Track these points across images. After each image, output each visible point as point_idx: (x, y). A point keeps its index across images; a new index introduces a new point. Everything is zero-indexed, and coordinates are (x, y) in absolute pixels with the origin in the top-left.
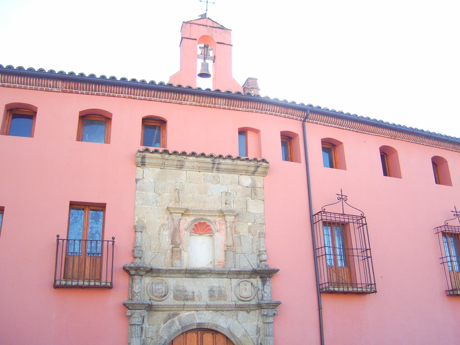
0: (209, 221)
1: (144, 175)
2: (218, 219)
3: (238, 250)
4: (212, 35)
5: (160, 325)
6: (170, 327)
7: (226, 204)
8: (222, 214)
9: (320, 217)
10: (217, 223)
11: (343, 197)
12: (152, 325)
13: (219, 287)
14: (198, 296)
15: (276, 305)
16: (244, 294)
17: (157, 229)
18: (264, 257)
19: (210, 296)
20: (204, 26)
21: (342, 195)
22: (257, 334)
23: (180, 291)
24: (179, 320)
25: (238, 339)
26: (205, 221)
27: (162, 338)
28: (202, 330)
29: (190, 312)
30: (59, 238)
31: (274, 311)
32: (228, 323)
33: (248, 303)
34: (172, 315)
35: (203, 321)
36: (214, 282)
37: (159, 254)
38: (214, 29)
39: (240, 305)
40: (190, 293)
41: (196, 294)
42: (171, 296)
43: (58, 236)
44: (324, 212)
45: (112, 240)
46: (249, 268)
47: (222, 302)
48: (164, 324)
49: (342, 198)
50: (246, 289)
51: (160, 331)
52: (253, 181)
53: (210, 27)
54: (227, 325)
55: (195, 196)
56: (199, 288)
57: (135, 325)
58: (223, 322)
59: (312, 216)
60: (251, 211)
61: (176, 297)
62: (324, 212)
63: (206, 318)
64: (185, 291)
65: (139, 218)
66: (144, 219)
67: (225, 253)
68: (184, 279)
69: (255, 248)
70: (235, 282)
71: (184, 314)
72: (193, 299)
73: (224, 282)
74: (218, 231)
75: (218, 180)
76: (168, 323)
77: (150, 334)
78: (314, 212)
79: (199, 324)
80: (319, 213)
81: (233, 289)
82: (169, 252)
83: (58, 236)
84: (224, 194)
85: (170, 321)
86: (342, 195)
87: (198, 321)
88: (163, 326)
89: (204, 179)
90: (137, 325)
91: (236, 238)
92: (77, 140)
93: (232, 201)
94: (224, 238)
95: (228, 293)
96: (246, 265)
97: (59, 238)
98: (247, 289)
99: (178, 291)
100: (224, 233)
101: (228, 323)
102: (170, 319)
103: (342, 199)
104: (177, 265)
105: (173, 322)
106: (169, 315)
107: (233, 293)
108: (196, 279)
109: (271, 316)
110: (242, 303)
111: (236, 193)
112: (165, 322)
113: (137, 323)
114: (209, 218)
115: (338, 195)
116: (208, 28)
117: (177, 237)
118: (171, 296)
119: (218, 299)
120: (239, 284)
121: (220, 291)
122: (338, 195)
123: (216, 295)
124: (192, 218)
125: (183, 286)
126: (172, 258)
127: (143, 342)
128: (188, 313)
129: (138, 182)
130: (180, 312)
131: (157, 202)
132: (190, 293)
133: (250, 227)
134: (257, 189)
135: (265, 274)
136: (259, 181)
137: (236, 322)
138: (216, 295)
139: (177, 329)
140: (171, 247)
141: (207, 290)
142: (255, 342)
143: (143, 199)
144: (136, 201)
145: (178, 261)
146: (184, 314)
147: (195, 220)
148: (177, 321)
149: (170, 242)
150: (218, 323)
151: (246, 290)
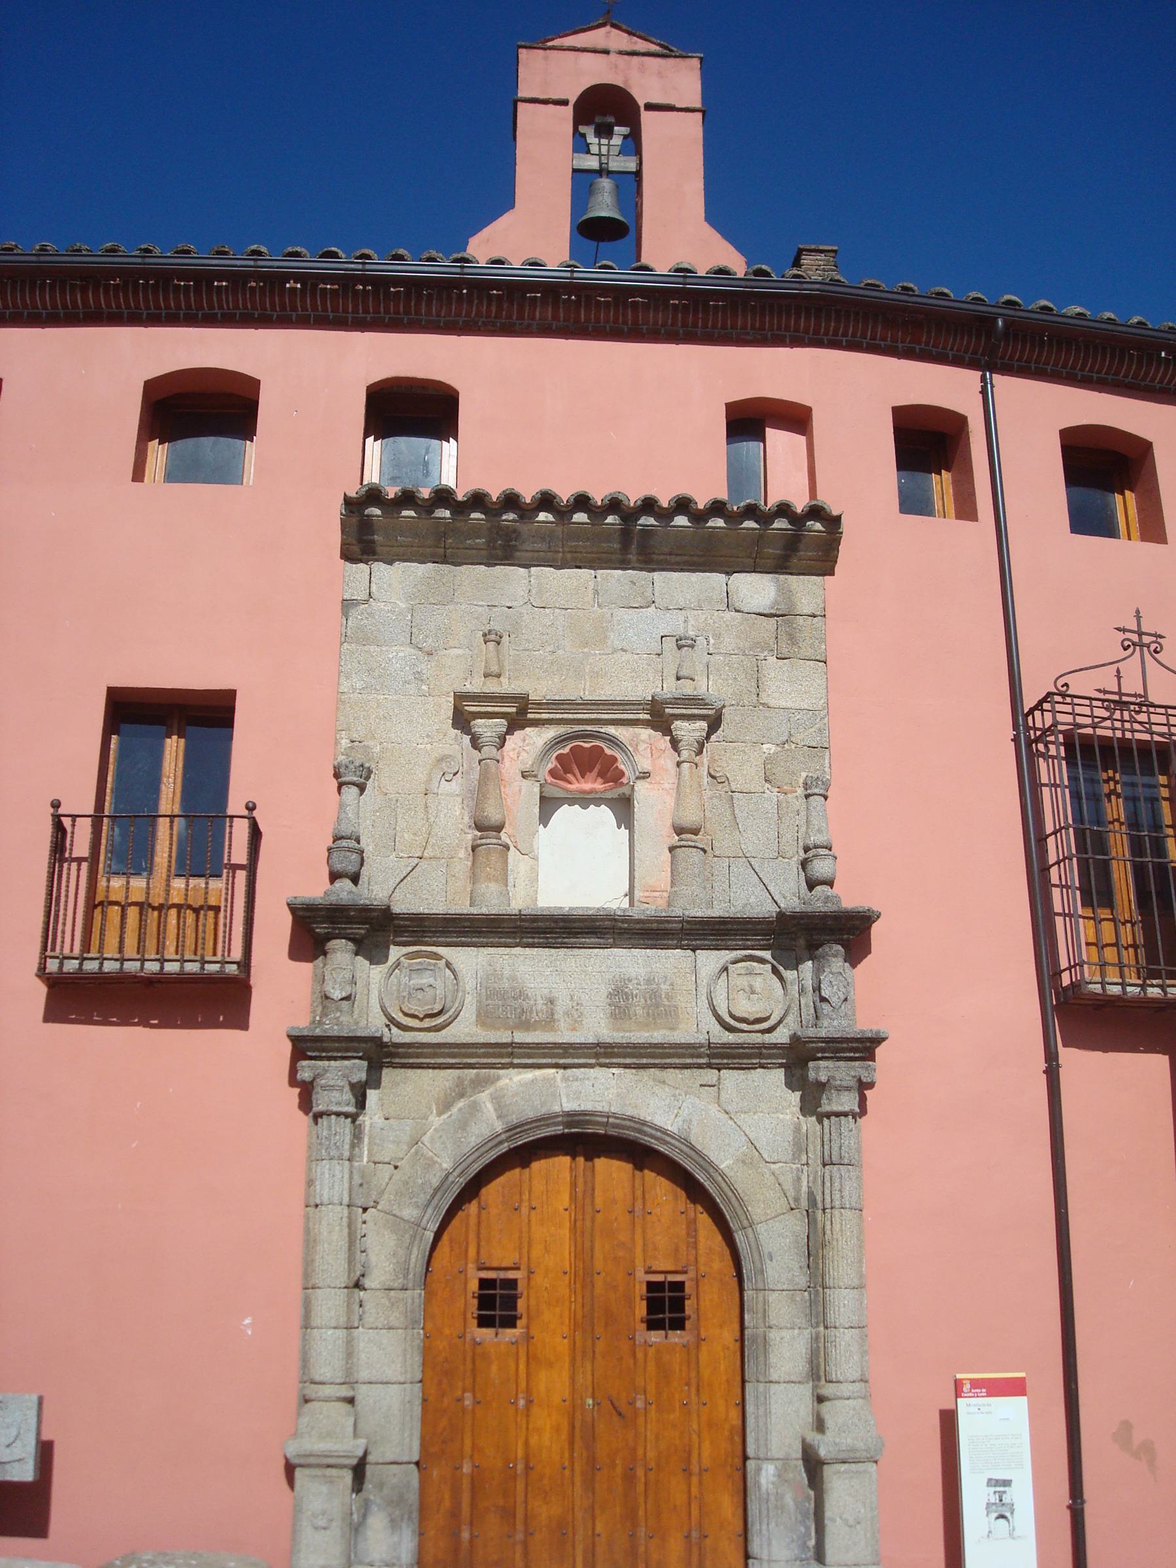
0: (613, 741)
1: (374, 588)
2: (645, 733)
3: (724, 843)
4: (626, 81)
5: (425, 1117)
6: (463, 1125)
7: (678, 679)
8: (659, 716)
9: (1048, 717)
10: (643, 747)
11: (1146, 639)
12: (398, 1118)
13: (649, 981)
14: (567, 1014)
15: (865, 1047)
16: (746, 1007)
17: (421, 775)
18: (821, 868)
19: (613, 1015)
20: (595, 51)
21: (1140, 634)
22: (795, 1157)
23: (501, 995)
24: (497, 1100)
25: (723, 1175)
26: (598, 743)
27: (430, 1164)
28: (584, 1140)
29: (538, 1073)
30: (61, 811)
31: (857, 1069)
32: (684, 1113)
33: (758, 1038)
34: (472, 1081)
35: (587, 1106)
36: (634, 963)
37: (423, 863)
38: (635, 59)
39: (725, 1046)
40: (540, 1002)
41: (560, 1009)
42: (469, 1014)
43: (56, 805)
44: (1064, 695)
45: (246, 813)
46: (767, 910)
47: (658, 1036)
48: (440, 1114)
49: (1141, 642)
50: (751, 986)
51: (426, 1139)
52: (785, 593)
53: (621, 53)
54: (679, 1119)
55: (561, 652)
56: (575, 988)
57: (328, 1114)
58: (659, 1104)
59: (1019, 715)
60: (772, 703)
61: (484, 1018)
62: (1064, 695)
63: (599, 1093)
64: (521, 995)
65: (355, 736)
66: (371, 743)
67: (673, 857)
68: (518, 950)
69: (788, 836)
70: (710, 960)
71: (516, 1079)
72: (549, 1022)
73: (668, 963)
74: (645, 776)
75: (649, 593)
76: (455, 1110)
77: (387, 1152)
78: (1029, 702)
79: (573, 1118)
80: (1044, 700)
81: (703, 991)
82: (462, 854)
83: (56, 805)
84: (670, 644)
85: (461, 1104)
86: (1140, 634)
87: (569, 1106)
88: (436, 1121)
89: (596, 592)
90: (338, 1114)
91: (715, 801)
92: (133, 480)
93: (700, 668)
94: (670, 801)
95: (683, 1001)
96: (752, 900)
97: (61, 811)
98: (759, 992)
99: (492, 994)
100: (669, 782)
101: (684, 1113)
102: (462, 1095)
103: (1142, 646)
104: (491, 903)
105: (475, 1108)
106: (460, 1081)
107: (703, 1000)
108: (562, 952)
109: (848, 1089)
110: (730, 1038)
111: (718, 636)
112: (445, 1106)
113: (335, 1109)
114: (611, 730)
115: (1124, 630)
116: (613, 57)
117: (492, 801)
118: (469, 1014)
119: (646, 1026)
120: (726, 969)
121: (655, 994)
122: (1124, 630)
123: (640, 1011)
124: (551, 732)
125: (513, 978)
126: (474, 877)
127: (362, 1177)
128: (529, 1075)
129: (354, 613)
130: (501, 1072)
131: (419, 677)
132: (540, 1002)
133: (769, 760)
134: (800, 620)
135: (822, 933)
136: (806, 590)
137: (714, 1109)
138: (640, 1011)
139: (486, 1132)
140: (470, 837)
141: (604, 990)
142: (788, 1186)
143: (370, 671)
144: (343, 679)
145: (493, 887)
146: (516, 1079)
147: (560, 741)
148: (489, 1105)
149: (466, 819)
150: (645, 1114)
151: (753, 992)
